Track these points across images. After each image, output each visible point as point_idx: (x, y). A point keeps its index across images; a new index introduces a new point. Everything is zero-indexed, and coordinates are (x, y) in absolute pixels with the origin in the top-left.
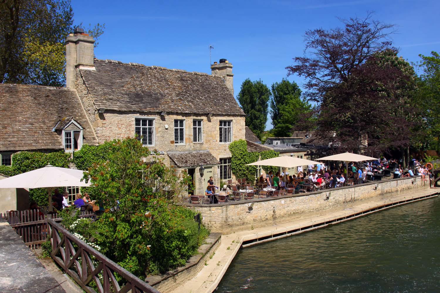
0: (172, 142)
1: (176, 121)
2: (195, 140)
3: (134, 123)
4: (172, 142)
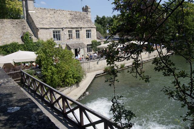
0: (68, 39)
1: (69, 31)
2: (77, 38)
3: (52, 32)
4: (68, 39)
